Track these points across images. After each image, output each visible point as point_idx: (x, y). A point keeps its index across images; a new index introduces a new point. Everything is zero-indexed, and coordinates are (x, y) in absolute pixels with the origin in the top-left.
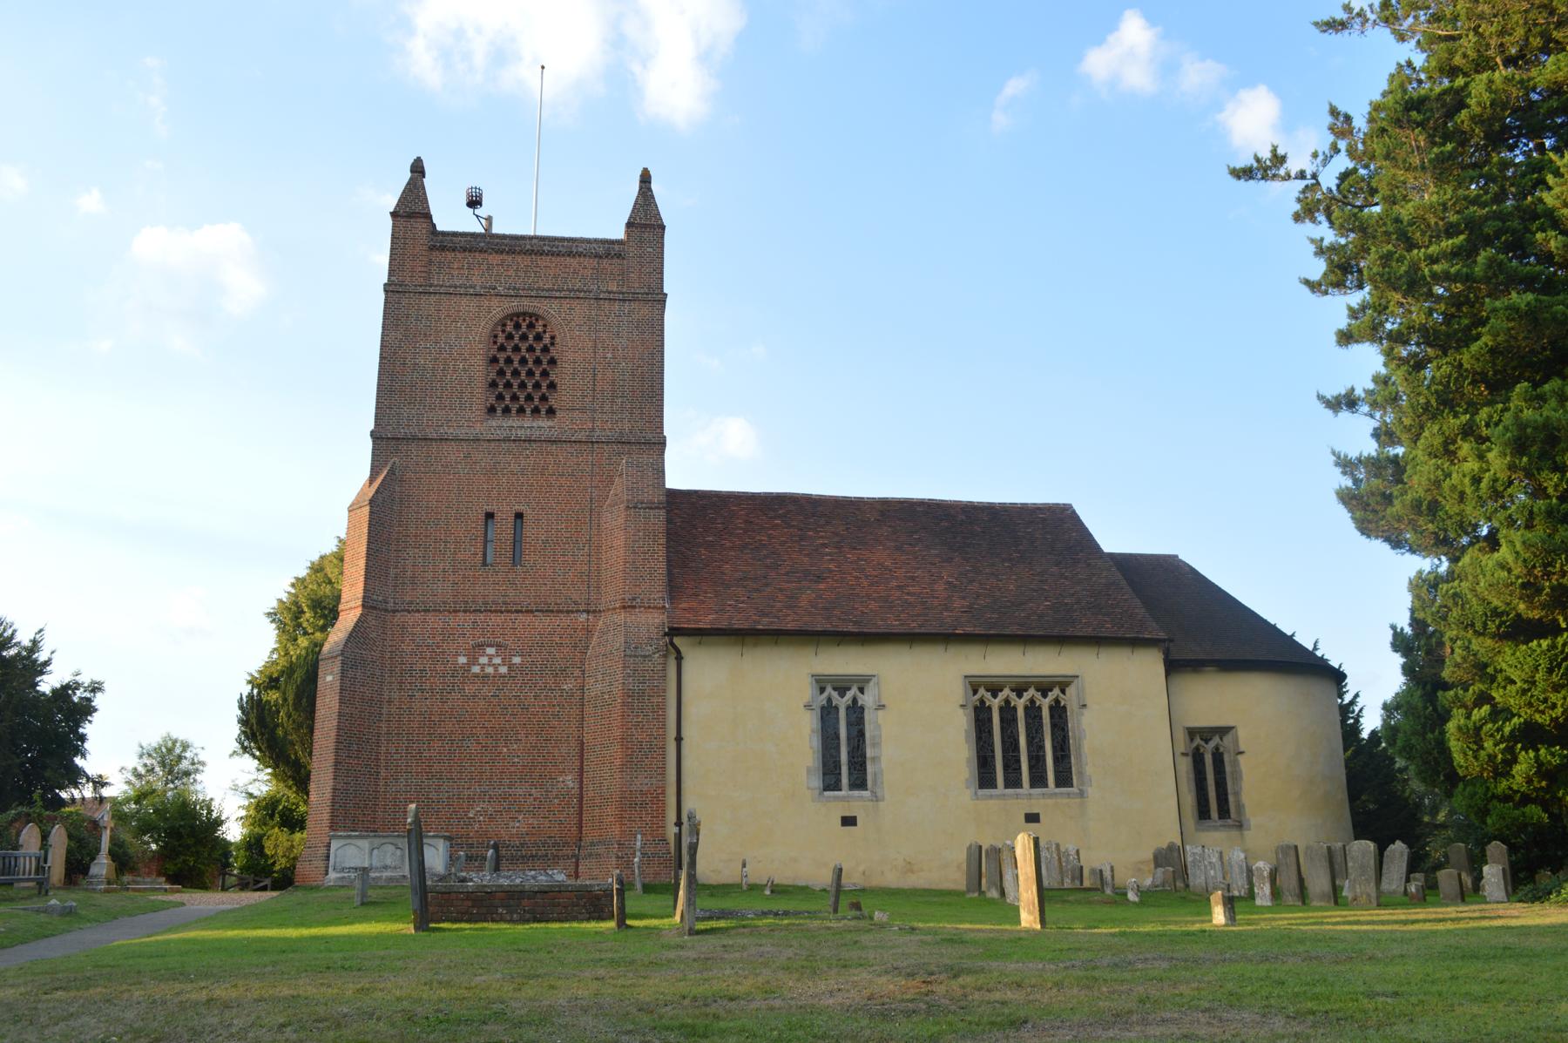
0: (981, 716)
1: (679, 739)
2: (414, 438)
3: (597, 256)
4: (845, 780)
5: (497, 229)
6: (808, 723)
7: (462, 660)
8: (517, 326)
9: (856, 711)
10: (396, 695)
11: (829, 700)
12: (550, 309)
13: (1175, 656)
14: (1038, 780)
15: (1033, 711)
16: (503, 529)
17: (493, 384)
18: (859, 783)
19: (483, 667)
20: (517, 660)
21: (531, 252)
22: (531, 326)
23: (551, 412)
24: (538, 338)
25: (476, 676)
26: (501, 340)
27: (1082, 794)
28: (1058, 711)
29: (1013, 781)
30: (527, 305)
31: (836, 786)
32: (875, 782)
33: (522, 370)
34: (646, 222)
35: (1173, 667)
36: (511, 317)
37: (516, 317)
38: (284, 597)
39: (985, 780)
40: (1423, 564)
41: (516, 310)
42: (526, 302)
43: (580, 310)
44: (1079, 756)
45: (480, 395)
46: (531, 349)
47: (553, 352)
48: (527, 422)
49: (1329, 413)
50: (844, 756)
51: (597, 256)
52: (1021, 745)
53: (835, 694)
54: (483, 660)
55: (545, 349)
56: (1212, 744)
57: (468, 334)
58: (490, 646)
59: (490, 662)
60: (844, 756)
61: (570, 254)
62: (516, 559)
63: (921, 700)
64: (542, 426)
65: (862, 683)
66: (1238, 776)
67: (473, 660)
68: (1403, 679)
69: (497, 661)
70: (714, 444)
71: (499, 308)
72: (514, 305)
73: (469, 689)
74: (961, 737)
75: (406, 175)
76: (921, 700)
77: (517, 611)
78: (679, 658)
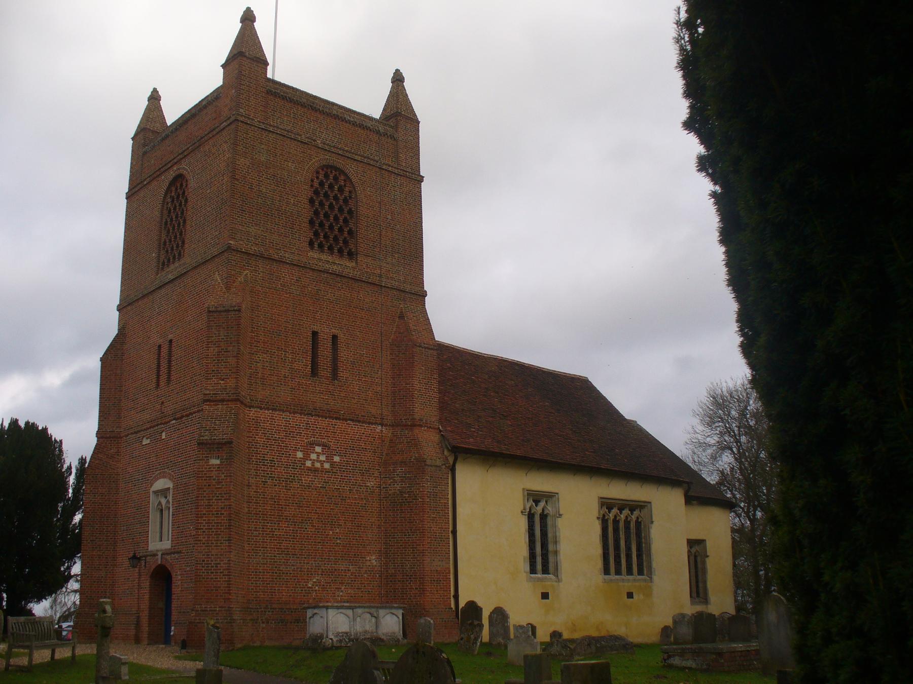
2: (262, 256)
7: (300, 455)
8: (326, 176)
9: (544, 517)
10: (252, 481)
12: (351, 169)
13: (691, 493)
14: (630, 572)
18: (545, 570)
19: (313, 462)
20: (337, 459)
22: (336, 179)
23: (351, 255)
24: (341, 190)
25: (309, 469)
26: (316, 184)
30: (340, 163)
32: (557, 569)
34: (400, 112)
37: (328, 168)
39: (606, 571)
41: (331, 163)
47: (351, 203)
48: (324, 257)
50: (541, 555)
52: (625, 545)
55: (346, 201)
58: (319, 445)
59: (317, 457)
64: (345, 265)
65: (549, 496)
67: (306, 457)
69: (323, 458)
71: (318, 159)
73: (306, 480)
75: (236, 27)
76: (579, 504)
77: (336, 418)
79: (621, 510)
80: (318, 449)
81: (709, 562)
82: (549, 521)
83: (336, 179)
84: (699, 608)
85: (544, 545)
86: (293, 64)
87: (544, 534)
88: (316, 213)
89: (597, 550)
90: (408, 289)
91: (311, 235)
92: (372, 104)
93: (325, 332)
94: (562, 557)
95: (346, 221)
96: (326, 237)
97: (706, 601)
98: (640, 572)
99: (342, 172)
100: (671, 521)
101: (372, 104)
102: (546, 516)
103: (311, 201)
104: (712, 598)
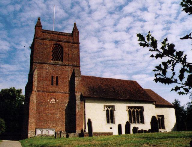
0: (130, 112)
3: (69, 36)
8: (56, 46)
11: (107, 109)
16: (55, 80)
19: (52, 102)
21: (58, 34)
31: (109, 123)
33: (58, 54)
36: (55, 44)
37: (56, 44)
38: (15, 89)
42: (57, 42)
43: (66, 44)
49: (137, 36)
50: (110, 118)
51: (69, 36)
53: (108, 108)
54: (52, 101)
57: (49, 46)
60: (110, 118)
61: (64, 35)
63: (122, 112)
65: (113, 107)
67: (50, 101)
68: (162, 67)
70: (90, 67)
71: (53, 42)
74: (127, 115)
76: (122, 112)
80: (53, 99)
92: (69, 31)
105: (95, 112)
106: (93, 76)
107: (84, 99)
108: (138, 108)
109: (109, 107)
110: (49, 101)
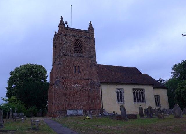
1: (102, 96)
4: (137, 101)
5: (69, 27)
6: (116, 94)
8: (77, 41)
9: (121, 92)
14: (141, 101)
15: (139, 93)
17: (74, 49)
18: (122, 102)
21: (78, 31)
22: (78, 41)
23: (82, 53)
24: (79, 43)
27: (145, 103)
28: (142, 93)
29: (138, 101)
30: (78, 38)
34: (91, 28)
35: (154, 88)
36: (76, 40)
37: (77, 40)
39: (135, 101)
40: (49, 68)
42: (78, 38)
44: (145, 98)
45: (73, 50)
46: (79, 44)
50: (120, 98)
52: (139, 96)
56: (157, 97)
59: (76, 86)
60: (120, 98)
62: (79, 72)
63: (128, 91)
65: (122, 89)
66: (160, 101)
67: (74, 86)
71: (74, 38)
72: (76, 38)
75: (89, 24)
76: (128, 91)
78: (101, 86)
79: (138, 90)
80: (77, 84)
81: (161, 99)
82: (122, 93)
83: (78, 41)
84: (157, 108)
85: (121, 97)
86: (72, 24)
87: (158, 100)
88: (75, 47)
89: (133, 98)
90: (93, 57)
91: (74, 51)
92: (86, 28)
93: (77, 66)
94: (124, 99)
95: (81, 48)
96: (77, 51)
97: (160, 106)
98: (143, 101)
99: (79, 40)
100: (149, 92)
101: (86, 28)
102: (121, 92)
103: (74, 45)
104: (162, 105)
105: (108, 95)
106: (168, 99)
107: (102, 83)
108: (141, 90)
109: (119, 89)
110: (74, 86)
